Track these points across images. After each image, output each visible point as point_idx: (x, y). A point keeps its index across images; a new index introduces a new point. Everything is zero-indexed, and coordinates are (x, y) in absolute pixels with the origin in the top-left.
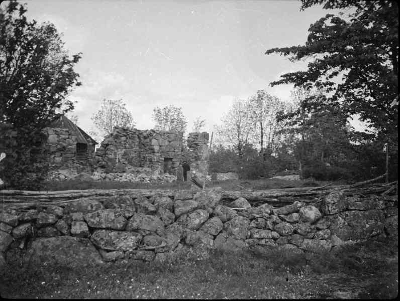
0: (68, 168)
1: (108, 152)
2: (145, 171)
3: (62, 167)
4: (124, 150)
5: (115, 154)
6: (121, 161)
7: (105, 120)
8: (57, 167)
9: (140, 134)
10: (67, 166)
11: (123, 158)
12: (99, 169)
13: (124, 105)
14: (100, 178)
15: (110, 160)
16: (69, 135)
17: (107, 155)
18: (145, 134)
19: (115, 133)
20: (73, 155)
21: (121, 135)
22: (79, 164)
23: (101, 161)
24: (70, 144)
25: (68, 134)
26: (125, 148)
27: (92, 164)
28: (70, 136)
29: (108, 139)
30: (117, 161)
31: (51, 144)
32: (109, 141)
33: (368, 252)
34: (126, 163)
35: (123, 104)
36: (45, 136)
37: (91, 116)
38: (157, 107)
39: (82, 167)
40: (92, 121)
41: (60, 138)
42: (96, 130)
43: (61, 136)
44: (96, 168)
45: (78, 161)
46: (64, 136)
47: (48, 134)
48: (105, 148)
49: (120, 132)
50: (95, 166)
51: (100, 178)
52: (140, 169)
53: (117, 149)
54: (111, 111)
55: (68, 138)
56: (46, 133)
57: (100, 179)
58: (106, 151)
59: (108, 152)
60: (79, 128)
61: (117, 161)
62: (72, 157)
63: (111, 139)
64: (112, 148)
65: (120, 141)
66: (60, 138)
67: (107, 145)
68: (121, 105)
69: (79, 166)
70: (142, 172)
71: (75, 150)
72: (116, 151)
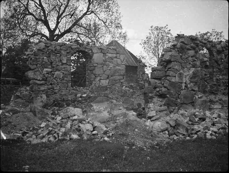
0: (107, 100)
1: (171, 73)
2: (220, 100)
3: (98, 99)
4: (193, 70)
5: (181, 75)
6: (189, 86)
7: (153, 45)
8: (90, 97)
9: (213, 46)
10: (106, 96)
11: (191, 82)
12: (155, 99)
13: (170, 30)
14: (166, 126)
15: (173, 84)
16: (117, 53)
17: (168, 78)
18: (219, 47)
19: (179, 45)
20: (122, 77)
21: (188, 47)
22: (128, 87)
23: (158, 87)
24: (118, 65)
25: (115, 52)
26: (194, 66)
27: (116, 49)
28: (118, 55)
29: (170, 53)
30: (183, 85)
31: (96, 65)
32: (171, 56)
33: (3, 26)
34: (196, 89)
35: (168, 30)
36: (89, 55)
37: (140, 42)
38: (199, 32)
39: (131, 90)
40: (141, 46)
41: (107, 57)
42: (145, 54)
43: (108, 54)
44: (152, 98)
45: (128, 84)
46: (110, 55)
47: (92, 52)
48: (165, 67)
49: (186, 42)
50: (150, 95)
51: (166, 126)
52: (212, 97)
53: (183, 68)
54: (158, 36)
55: (116, 57)
56: (90, 51)
57: (167, 129)
58: (166, 72)
59: (171, 73)
60: (129, 52)
61: (183, 87)
62: (120, 80)
63: (173, 53)
64: (176, 67)
65: (186, 56)
66: (107, 57)
67: (169, 62)
68: (166, 31)
69: (129, 91)
70: (217, 101)
71: (124, 71)
72: (181, 71)
